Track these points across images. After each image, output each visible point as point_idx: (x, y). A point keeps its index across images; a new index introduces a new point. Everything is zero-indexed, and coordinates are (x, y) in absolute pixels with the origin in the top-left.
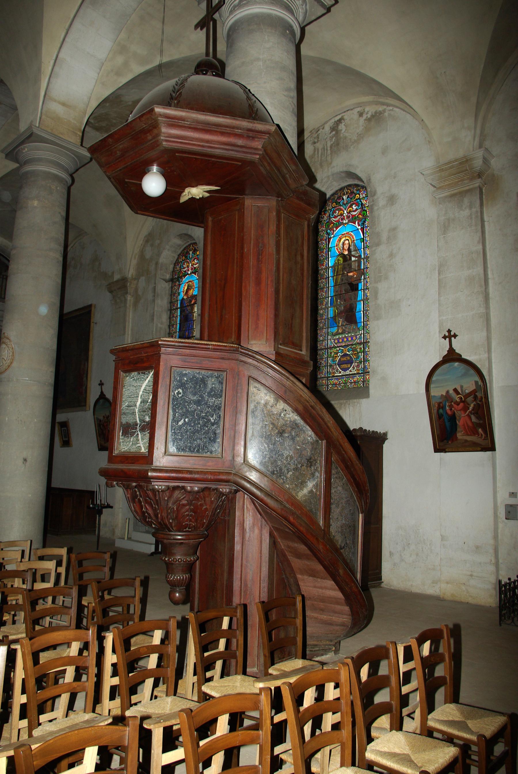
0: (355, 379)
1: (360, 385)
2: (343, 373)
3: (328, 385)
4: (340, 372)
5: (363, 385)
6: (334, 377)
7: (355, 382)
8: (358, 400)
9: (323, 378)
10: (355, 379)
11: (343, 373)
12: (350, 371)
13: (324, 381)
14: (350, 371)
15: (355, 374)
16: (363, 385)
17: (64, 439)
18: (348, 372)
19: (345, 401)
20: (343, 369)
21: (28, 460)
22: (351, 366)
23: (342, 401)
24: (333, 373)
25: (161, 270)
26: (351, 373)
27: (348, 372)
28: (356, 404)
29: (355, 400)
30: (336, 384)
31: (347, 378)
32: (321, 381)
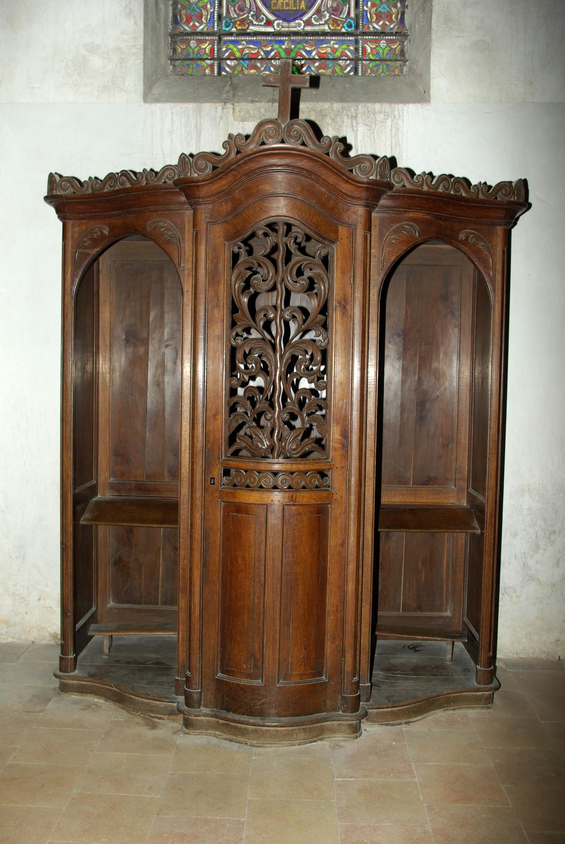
0: (325, 49)
1: (343, 68)
2: (278, 25)
3: (221, 59)
4: (269, 23)
5: (356, 70)
6: (249, 34)
7: (323, 58)
8: (386, 107)
9: (202, 34)
10: (325, 49)
11: (278, 25)
12: (308, 23)
13: (206, 47)
14: (308, 23)
15: (324, 34)
16: (356, 70)
17: (262, 24)
18: (298, 25)
19: (337, 106)
20: (279, 14)
21: (311, 233)
22: (309, 8)
23: (327, 105)
24: (243, 21)
25: (341, 522)
26: (308, 29)
27: (298, 25)
28: (380, 117)
29: (377, 106)
30: (252, 58)
31: (296, 43)
32: (193, 44)
